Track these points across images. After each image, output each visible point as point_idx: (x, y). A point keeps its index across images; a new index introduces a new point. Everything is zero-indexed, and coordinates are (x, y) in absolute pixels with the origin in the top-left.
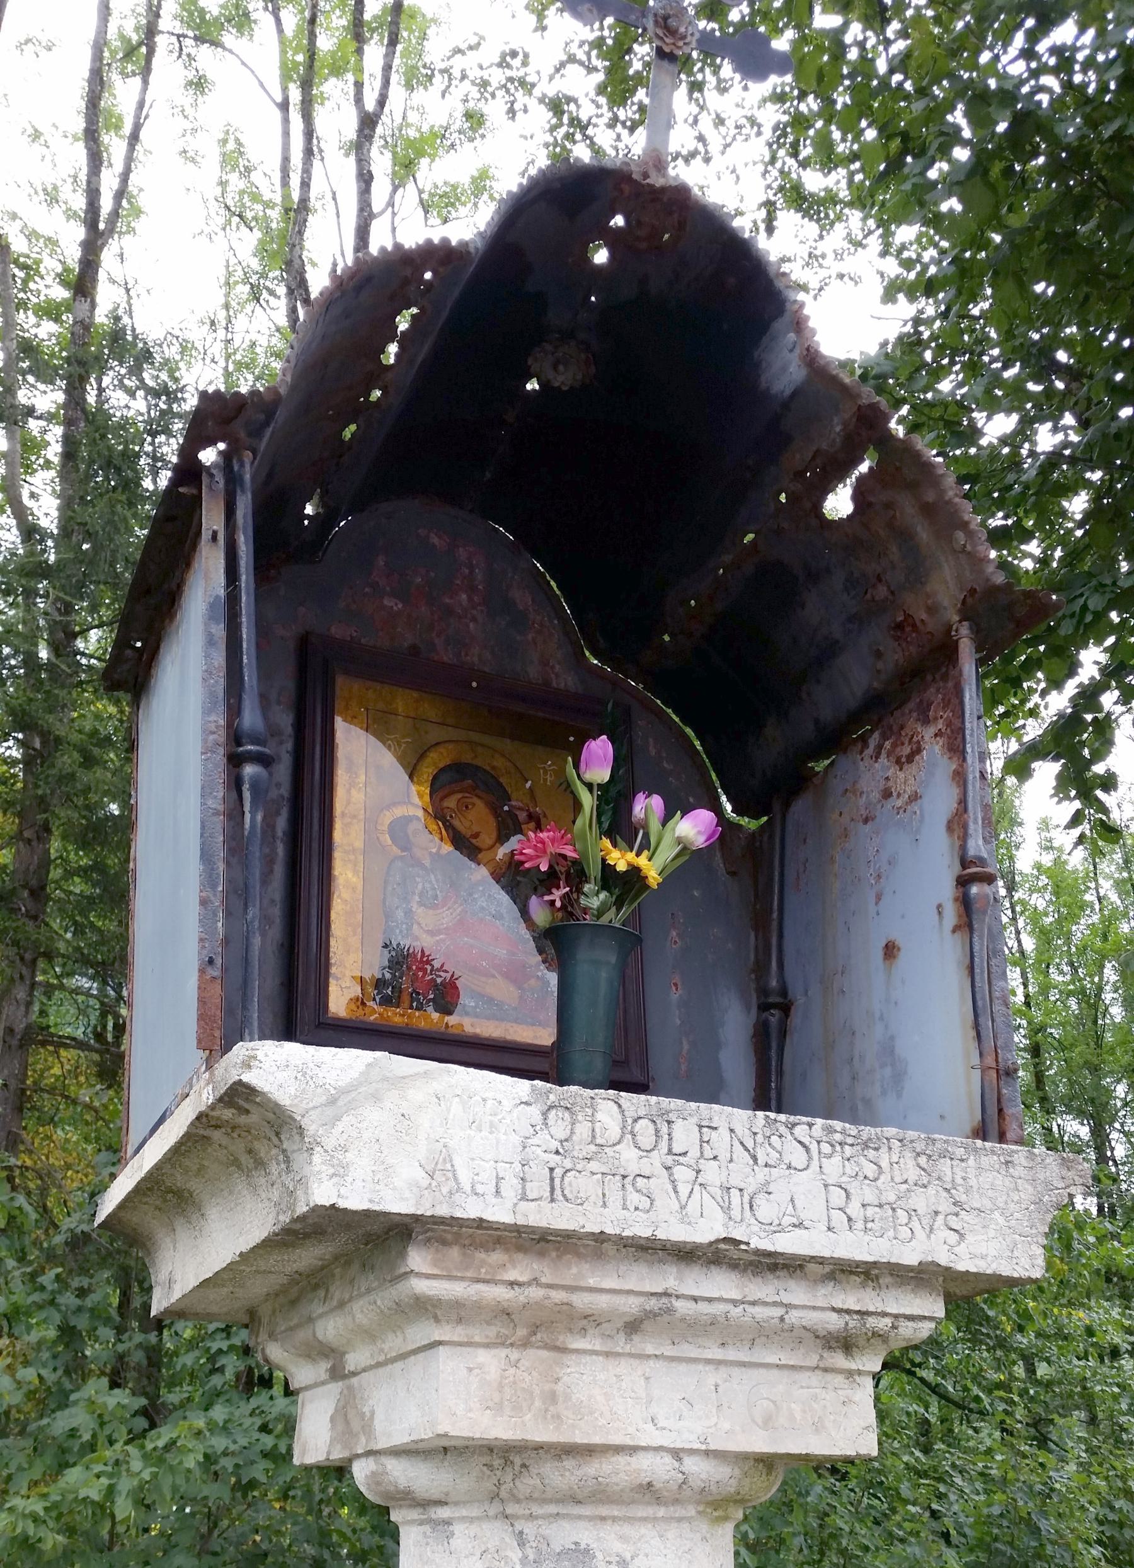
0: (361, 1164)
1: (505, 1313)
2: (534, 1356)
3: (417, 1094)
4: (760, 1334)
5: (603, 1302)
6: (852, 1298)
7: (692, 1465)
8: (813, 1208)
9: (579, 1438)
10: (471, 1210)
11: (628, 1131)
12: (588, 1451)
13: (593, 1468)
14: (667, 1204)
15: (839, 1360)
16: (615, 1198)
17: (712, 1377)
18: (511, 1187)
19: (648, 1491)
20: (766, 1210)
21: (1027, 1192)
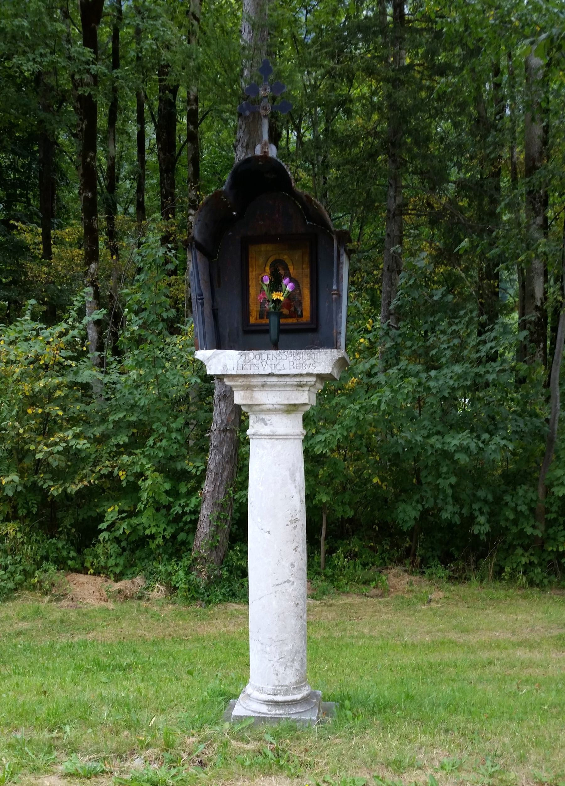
0: (213, 367)
1: (241, 386)
2: (248, 392)
3: (221, 356)
4: (286, 385)
5: (255, 383)
6: (298, 379)
7: (275, 406)
8: (287, 365)
9: (256, 403)
10: (229, 373)
11: (255, 357)
12: (259, 405)
13: (260, 407)
14: (261, 368)
15: (300, 388)
16: (252, 368)
17: (278, 393)
18: (236, 369)
19: (269, 410)
20: (278, 367)
21: (330, 358)
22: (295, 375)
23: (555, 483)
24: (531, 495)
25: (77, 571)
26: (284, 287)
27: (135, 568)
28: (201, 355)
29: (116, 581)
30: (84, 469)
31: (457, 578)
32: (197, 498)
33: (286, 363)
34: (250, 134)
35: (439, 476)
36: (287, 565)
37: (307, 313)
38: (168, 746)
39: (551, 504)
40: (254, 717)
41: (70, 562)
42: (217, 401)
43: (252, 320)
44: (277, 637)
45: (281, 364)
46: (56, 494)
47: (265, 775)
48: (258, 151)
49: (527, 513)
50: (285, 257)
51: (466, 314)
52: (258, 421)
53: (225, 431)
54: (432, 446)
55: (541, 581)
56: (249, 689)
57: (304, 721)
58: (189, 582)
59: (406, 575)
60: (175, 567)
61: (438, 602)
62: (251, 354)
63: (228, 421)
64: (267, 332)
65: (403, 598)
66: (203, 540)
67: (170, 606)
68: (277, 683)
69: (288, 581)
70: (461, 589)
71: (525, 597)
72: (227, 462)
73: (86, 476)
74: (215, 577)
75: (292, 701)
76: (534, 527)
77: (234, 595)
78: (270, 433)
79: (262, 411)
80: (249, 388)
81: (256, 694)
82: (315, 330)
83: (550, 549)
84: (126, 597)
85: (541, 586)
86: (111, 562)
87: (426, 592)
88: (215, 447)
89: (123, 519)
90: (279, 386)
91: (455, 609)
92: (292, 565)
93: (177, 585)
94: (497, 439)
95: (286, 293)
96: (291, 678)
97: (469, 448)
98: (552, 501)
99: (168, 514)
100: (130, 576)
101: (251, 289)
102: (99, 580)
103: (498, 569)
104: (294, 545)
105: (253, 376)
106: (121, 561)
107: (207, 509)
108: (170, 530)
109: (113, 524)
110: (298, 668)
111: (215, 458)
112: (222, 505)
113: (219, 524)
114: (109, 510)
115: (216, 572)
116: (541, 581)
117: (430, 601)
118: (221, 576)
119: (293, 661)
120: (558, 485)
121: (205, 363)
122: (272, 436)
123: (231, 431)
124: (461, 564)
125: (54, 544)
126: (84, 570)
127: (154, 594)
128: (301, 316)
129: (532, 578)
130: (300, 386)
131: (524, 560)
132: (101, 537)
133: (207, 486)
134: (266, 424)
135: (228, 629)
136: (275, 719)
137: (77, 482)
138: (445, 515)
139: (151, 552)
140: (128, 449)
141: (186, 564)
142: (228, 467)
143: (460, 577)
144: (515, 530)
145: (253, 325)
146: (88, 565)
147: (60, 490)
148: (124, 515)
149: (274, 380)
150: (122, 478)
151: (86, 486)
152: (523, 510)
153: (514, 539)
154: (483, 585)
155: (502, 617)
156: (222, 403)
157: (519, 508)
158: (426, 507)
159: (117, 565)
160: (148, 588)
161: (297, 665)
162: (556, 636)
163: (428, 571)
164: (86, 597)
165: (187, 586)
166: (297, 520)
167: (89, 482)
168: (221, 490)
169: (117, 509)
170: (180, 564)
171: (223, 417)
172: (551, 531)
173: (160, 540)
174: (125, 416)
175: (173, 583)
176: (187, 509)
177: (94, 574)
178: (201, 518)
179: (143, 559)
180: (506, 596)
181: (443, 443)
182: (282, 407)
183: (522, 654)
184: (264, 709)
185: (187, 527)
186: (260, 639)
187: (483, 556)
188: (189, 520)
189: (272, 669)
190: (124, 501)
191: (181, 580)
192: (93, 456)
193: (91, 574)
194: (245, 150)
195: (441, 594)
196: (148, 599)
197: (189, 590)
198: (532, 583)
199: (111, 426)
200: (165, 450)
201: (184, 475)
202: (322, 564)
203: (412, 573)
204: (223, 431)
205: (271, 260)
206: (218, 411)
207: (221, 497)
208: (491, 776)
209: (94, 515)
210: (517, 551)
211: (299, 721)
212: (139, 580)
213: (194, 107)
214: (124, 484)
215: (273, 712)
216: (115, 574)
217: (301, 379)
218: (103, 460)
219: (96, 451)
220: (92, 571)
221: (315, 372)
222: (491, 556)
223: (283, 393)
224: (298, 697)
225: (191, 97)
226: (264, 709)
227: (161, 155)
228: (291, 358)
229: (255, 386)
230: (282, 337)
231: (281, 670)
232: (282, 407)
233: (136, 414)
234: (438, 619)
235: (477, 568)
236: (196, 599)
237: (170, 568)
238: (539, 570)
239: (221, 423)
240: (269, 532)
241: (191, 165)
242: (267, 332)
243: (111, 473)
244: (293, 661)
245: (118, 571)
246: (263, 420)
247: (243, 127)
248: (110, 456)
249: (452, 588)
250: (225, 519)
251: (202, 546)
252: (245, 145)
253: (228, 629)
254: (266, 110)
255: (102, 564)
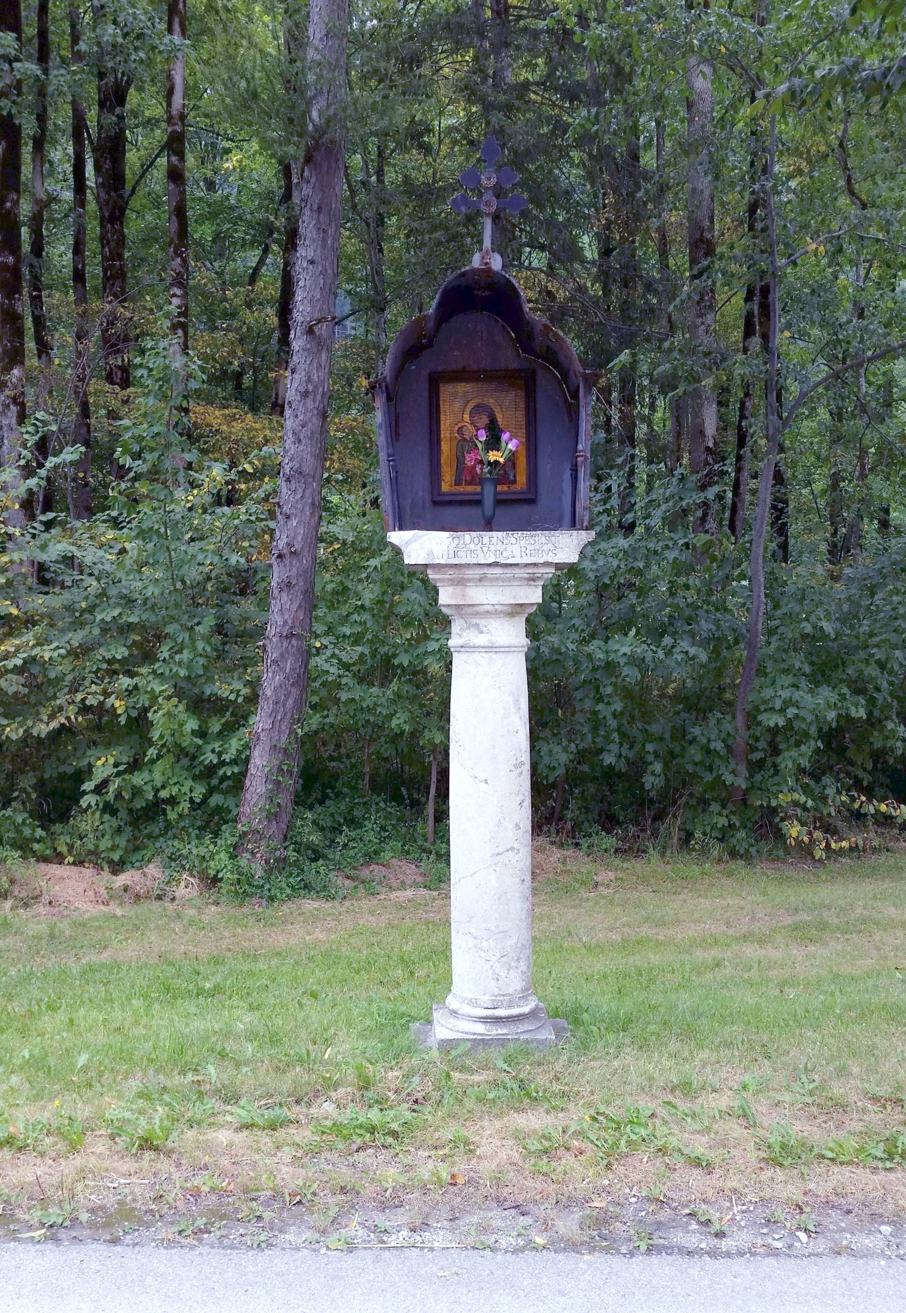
0: (413, 555)
4: (514, 578)
10: (437, 561)
11: (472, 540)
12: (473, 605)
14: (481, 555)
18: (445, 557)
20: (505, 554)
21: (576, 542)
22: (527, 565)
23: (762, 708)
24: (727, 726)
25: (45, 860)
26: (503, 444)
27: (144, 852)
28: (396, 537)
29: (115, 873)
30: (55, 697)
31: (625, 851)
32: (240, 740)
33: (516, 549)
34: (322, 190)
35: (600, 699)
36: (511, 826)
37: (522, 479)
38: (365, 1084)
39: (757, 739)
40: (468, 1040)
41: (36, 846)
42: (276, 592)
43: (445, 487)
44: (497, 926)
45: (509, 550)
46: (14, 737)
47: (517, 1110)
48: (476, 261)
49: (723, 752)
50: (492, 401)
51: (624, 463)
52: (468, 628)
53: (291, 635)
54: (589, 656)
55: (747, 851)
56: (452, 1001)
57: (538, 1041)
58: (238, 870)
59: (554, 848)
60: (211, 847)
61: (608, 886)
62: (467, 536)
63: (293, 623)
64: (478, 503)
65: (557, 882)
66: (255, 805)
67: (213, 908)
68: (497, 992)
69: (512, 849)
70: (637, 865)
71: (730, 874)
72: (293, 685)
73: (61, 709)
74: (275, 860)
75: (518, 1016)
76: (734, 772)
77: (307, 887)
78: (487, 644)
79: (477, 614)
80: (460, 582)
81: (466, 1009)
82: (532, 501)
83: (759, 803)
84: (138, 896)
85: (747, 857)
86: (105, 844)
87: (589, 872)
88: (275, 662)
89: (118, 774)
90: (503, 580)
91: (636, 895)
92: (517, 826)
93: (220, 875)
94: (684, 645)
95: (507, 452)
96: (515, 983)
97: (643, 659)
98: (758, 734)
99: (191, 767)
100: (137, 864)
101: (443, 443)
102: (88, 872)
103: (683, 834)
104: (519, 799)
105: (468, 566)
106: (122, 841)
107: (261, 757)
108: (199, 791)
109: (105, 783)
110: (525, 969)
111: (273, 678)
112: (285, 750)
113: (280, 778)
114: (99, 763)
115: (278, 853)
116: (747, 851)
117: (597, 885)
118: (285, 859)
119: (518, 960)
120: (766, 710)
121: (403, 549)
122: (490, 649)
123: (299, 637)
124: (632, 829)
125: (9, 818)
126: (59, 858)
127: (181, 891)
128: (514, 482)
129: (734, 847)
130: (533, 579)
131: (722, 821)
132: (84, 802)
133: (260, 721)
134: (482, 632)
135: (315, 936)
136: (502, 1042)
137: (45, 718)
138: (609, 759)
139: (168, 826)
140: (127, 668)
141: (229, 842)
142: (295, 691)
143: (630, 848)
144: (708, 777)
145: (445, 494)
146: (63, 849)
147: (21, 731)
148: (122, 768)
149: (497, 571)
150: (119, 712)
151: (63, 725)
152: (718, 748)
153: (705, 791)
154: (666, 859)
155: (706, 904)
156: (284, 594)
157: (712, 745)
158: (581, 747)
159: (114, 848)
160: (169, 882)
161: (523, 965)
162: (789, 926)
163: (585, 843)
164: (71, 899)
165: (236, 876)
166: (522, 764)
167: (68, 718)
168: (283, 727)
169: (111, 761)
170: (219, 842)
171: (286, 616)
172: (758, 777)
173: (185, 806)
174: (120, 614)
175: (212, 873)
176: (227, 757)
177: (74, 864)
178: (252, 770)
179: (156, 838)
180: (703, 873)
181: (607, 652)
182: (506, 608)
183: (750, 951)
184: (480, 1028)
185: (224, 785)
186: (473, 930)
187: (659, 817)
188: (229, 773)
189: (490, 972)
190: (121, 748)
191: (226, 866)
192: (69, 678)
193: (69, 864)
194: (315, 216)
195: (611, 875)
196: (173, 899)
197: (239, 881)
198: (734, 854)
199: (96, 631)
200: (188, 668)
201: (217, 705)
202: (430, 836)
203: (561, 846)
204: (287, 637)
205: (471, 405)
206: (278, 606)
207: (284, 738)
208: (811, 1093)
209: (70, 770)
210: (711, 808)
211: (532, 1041)
212: (153, 869)
213: (178, 128)
214: (123, 720)
215: (494, 1032)
216: (111, 862)
217: (535, 570)
218: (87, 683)
219: (73, 670)
220: (71, 859)
221: (556, 560)
222: (674, 816)
223: (508, 589)
224: (526, 1009)
225: (174, 112)
226: (480, 1028)
227: (103, 195)
228: (523, 543)
229: (469, 580)
230: (500, 511)
231: (503, 973)
232: (506, 608)
233: (137, 612)
234: (618, 909)
235: (655, 834)
236: (251, 895)
237: (202, 851)
238: (742, 834)
239: (284, 626)
240: (486, 781)
241: (174, 218)
242: (478, 503)
243: (101, 703)
244: (518, 960)
245: (116, 857)
246: (477, 625)
247: (313, 180)
248: (98, 678)
249: (625, 865)
250: (290, 772)
251: (254, 813)
252: (315, 207)
253: (315, 936)
254: (490, 206)
255: (91, 847)
